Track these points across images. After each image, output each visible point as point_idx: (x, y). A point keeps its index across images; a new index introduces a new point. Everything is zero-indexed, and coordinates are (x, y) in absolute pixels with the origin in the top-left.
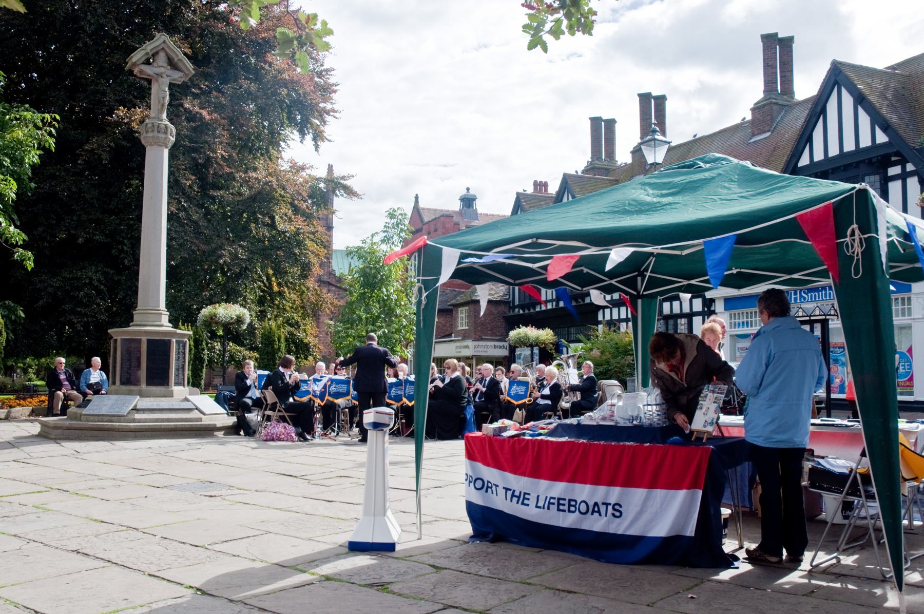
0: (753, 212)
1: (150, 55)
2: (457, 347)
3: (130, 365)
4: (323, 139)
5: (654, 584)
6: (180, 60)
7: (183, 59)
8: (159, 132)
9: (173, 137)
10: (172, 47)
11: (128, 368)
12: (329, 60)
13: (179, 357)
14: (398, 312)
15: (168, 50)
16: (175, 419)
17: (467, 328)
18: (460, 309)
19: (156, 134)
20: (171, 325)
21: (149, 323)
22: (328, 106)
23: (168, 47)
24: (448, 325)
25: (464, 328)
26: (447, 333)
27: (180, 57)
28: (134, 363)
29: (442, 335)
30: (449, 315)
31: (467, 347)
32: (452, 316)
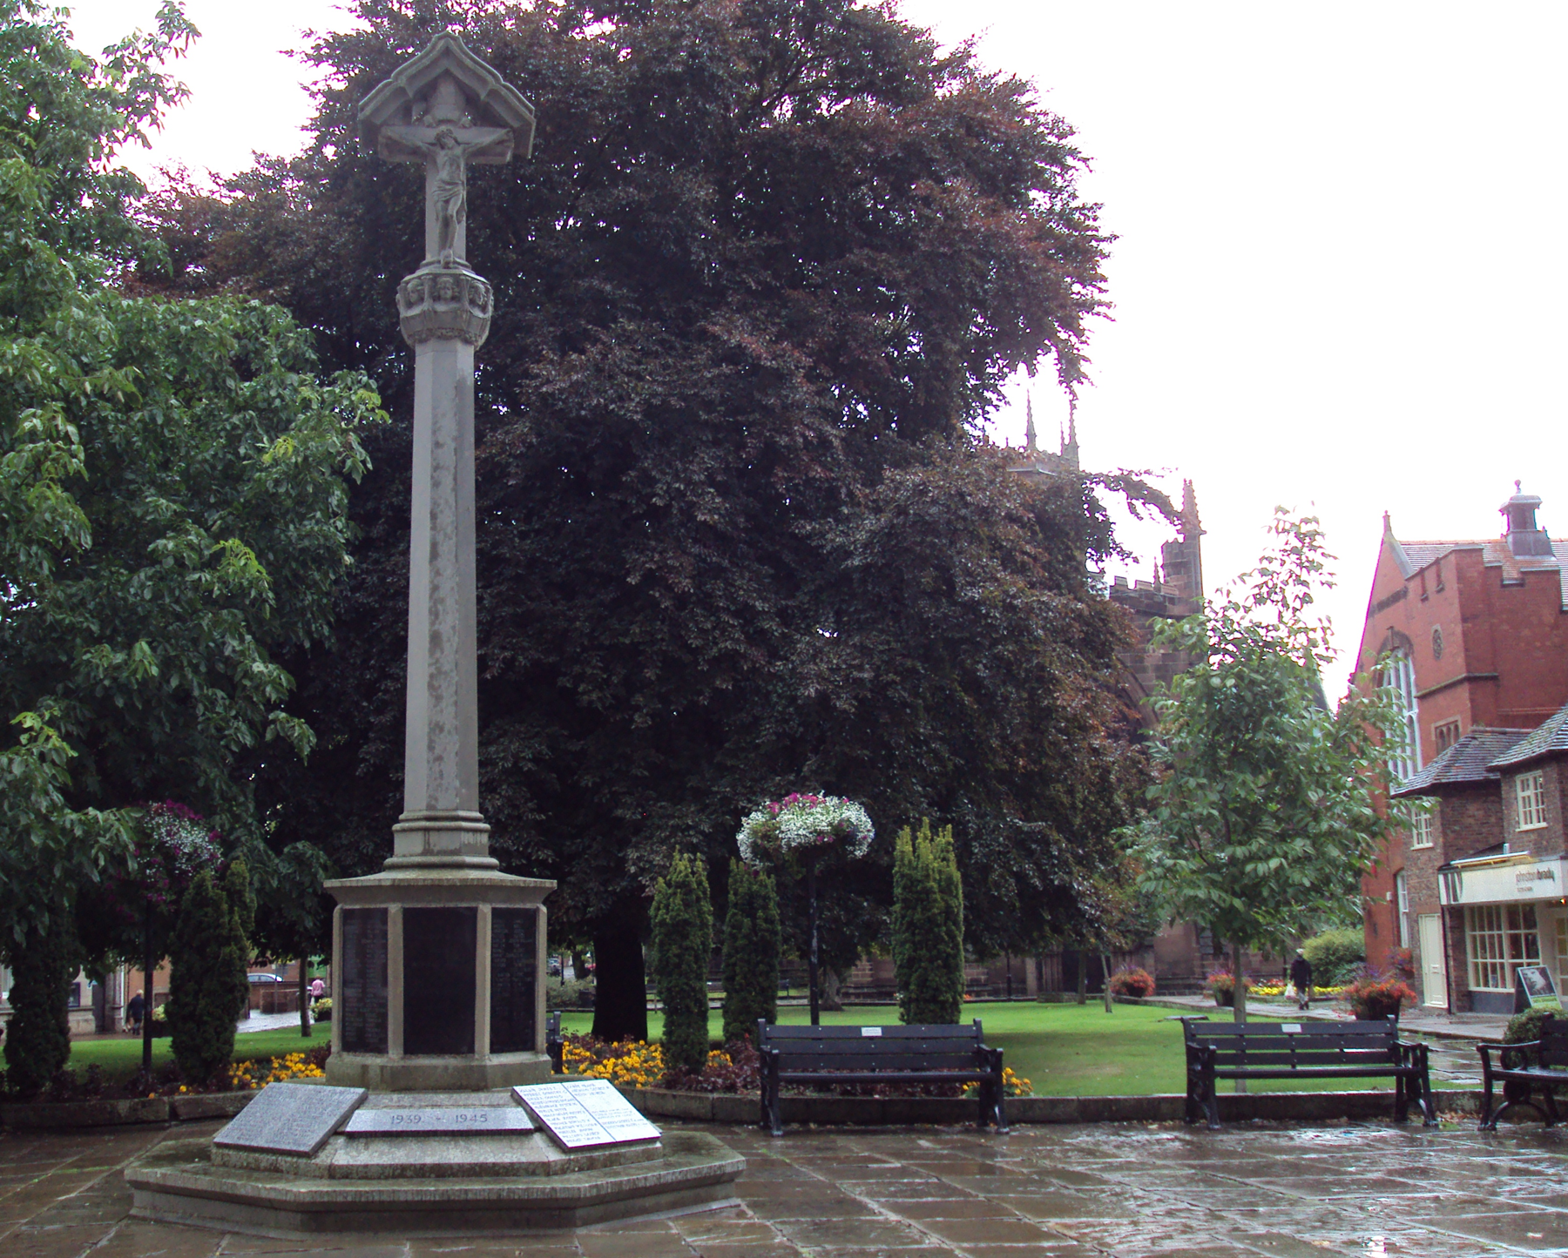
1: (411, 94)
2: (1520, 878)
4: (1081, 377)
6: (493, 93)
7: (504, 92)
9: (484, 309)
10: (468, 62)
12: (1085, 187)
14: (1314, 796)
16: (460, 1166)
17: (1544, 824)
18: (1519, 778)
20: (494, 861)
21: (469, 859)
22: (1090, 293)
23: (461, 64)
24: (1493, 820)
25: (1536, 825)
26: (1492, 841)
29: (1480, 847)
30: (1492, 795)
31: (1549, 875)
32: (1501, 798)
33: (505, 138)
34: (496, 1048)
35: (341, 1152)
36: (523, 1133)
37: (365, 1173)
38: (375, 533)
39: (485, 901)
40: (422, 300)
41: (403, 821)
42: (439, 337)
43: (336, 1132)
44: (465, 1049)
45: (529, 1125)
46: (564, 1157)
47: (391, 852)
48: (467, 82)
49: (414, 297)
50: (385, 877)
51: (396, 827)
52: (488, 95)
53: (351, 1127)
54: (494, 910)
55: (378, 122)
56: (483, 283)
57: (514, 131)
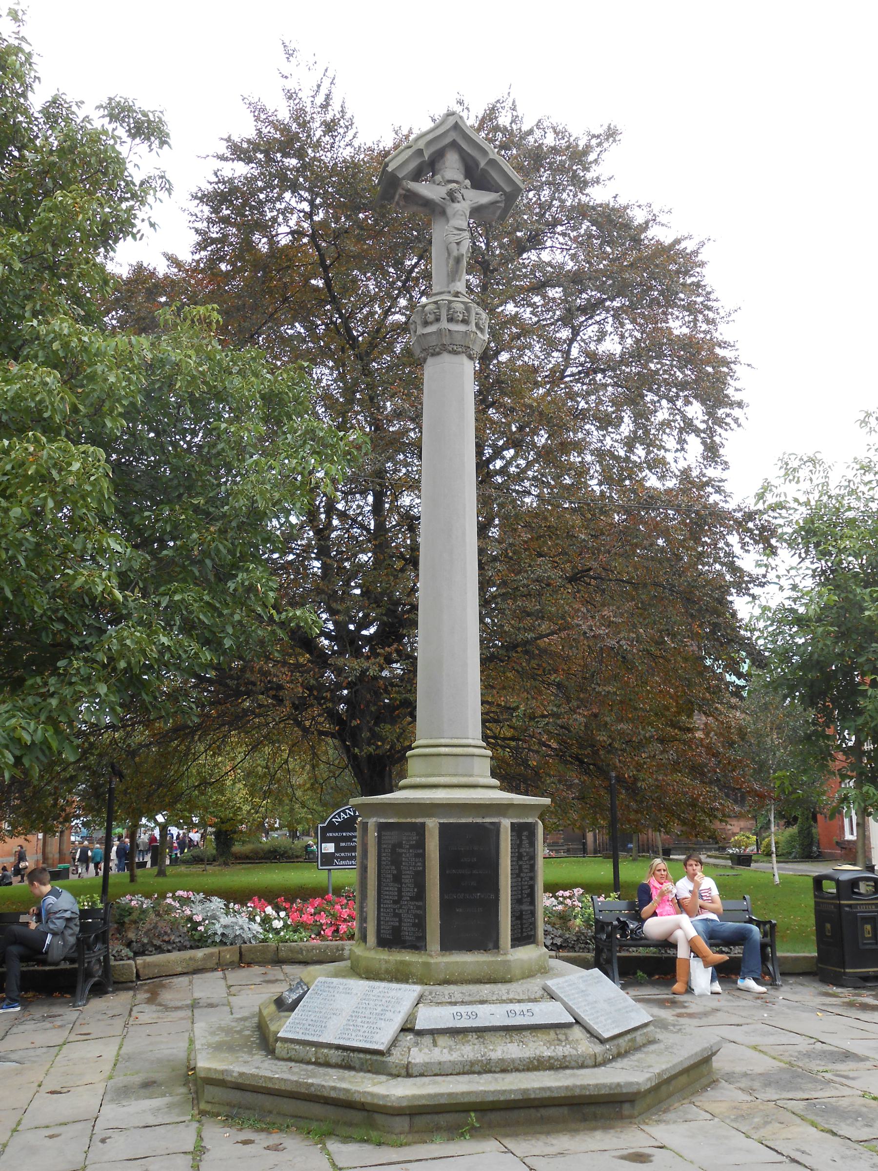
0: (535, 1133)
3: (400, 891)
5: (288, 1127)
8: (451, 320)
11: (395, 902)
13: (520, 867)
15: (464, 146)
19: (444, 324)
20: (496, 782)
27: (491, 156)
28: (409, 890)
35: (414, 1051)
38: (531, 458)
40: (438, 320)
41: (417, 747)
42: (450, 352)
43: (406, 1029)
44: (491, 945)
49: (431, 318)
51: (409, 753)
52: (487, 164)
54: (442, 825)
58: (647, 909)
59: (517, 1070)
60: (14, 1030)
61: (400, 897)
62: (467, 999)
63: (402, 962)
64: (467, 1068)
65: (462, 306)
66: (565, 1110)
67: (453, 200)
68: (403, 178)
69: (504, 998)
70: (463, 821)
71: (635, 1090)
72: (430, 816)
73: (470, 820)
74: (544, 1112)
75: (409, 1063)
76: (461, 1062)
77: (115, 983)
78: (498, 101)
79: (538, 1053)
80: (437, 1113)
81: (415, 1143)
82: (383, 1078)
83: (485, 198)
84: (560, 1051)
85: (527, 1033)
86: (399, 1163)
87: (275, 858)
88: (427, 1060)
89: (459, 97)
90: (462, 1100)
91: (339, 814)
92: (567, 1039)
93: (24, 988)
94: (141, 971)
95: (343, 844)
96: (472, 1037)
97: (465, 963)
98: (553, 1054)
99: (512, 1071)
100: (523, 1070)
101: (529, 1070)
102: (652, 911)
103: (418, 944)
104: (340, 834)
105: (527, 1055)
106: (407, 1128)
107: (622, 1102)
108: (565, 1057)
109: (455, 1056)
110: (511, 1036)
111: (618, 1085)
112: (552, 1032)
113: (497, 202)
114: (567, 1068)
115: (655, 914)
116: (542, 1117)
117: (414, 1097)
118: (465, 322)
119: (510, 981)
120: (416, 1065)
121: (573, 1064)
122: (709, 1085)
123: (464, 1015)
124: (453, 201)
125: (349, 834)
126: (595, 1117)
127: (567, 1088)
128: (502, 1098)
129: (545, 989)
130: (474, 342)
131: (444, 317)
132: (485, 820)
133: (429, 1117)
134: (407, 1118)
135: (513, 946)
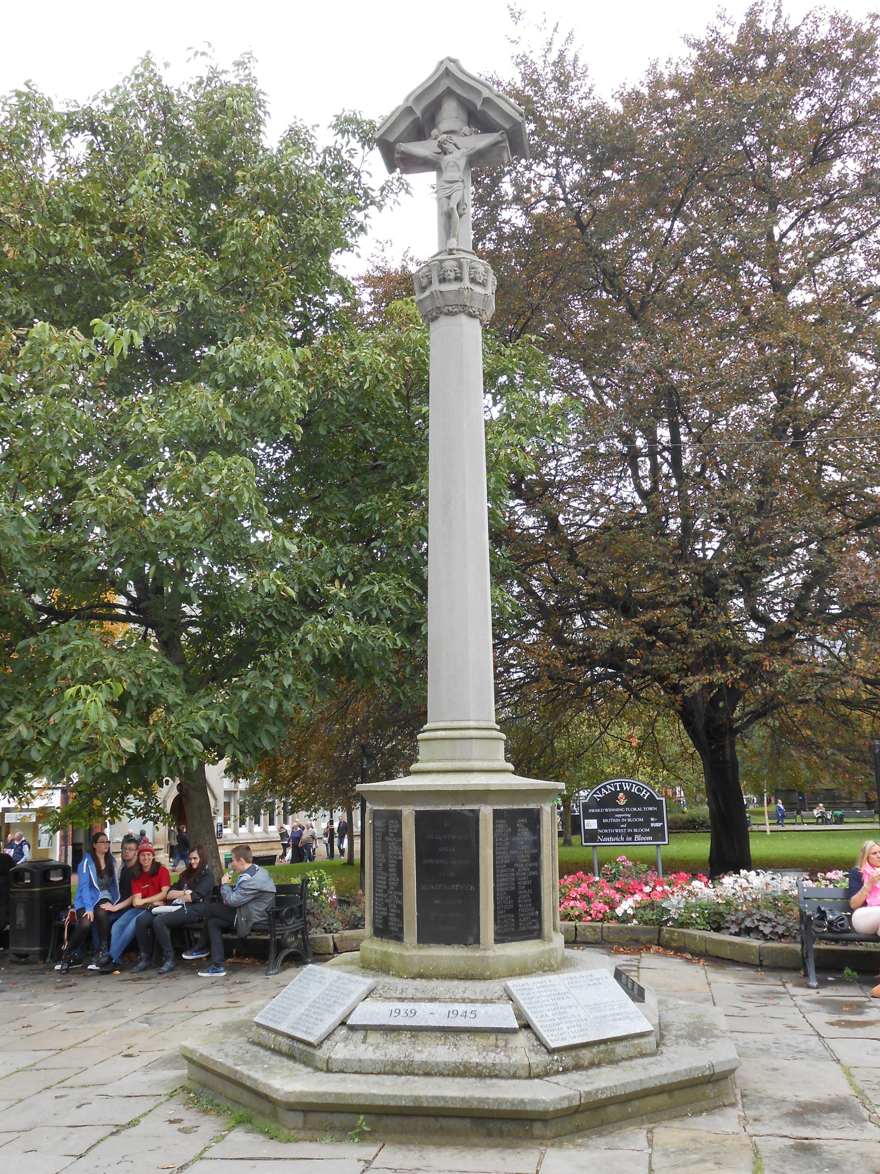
15: (458, 90)
27: (485, 95)
33: (500, 139)
34: (502, 937)
36: (513, 1031)
37: (360, 1069)
39: (486, 803)
42: (446, 314)
43: (343, 1023)
44: (471, 940)
45: (515, 1025)
46: (548, 1058)
47: (413, 759)
48: (464, 95)
50: (402, 783)
51: (419, 736)
53: (349, 1022)
54: (495, 812)
55: (391, 139)
56: (483, 265)
57: (507, 132)
58: (856, 898)
59: (442, 1075)
60: (203, 991)
61: (388, 885)
62: (419, 995)
63: (385, 954)
64: (388, 1068)
65: (454, 263)
66: (468, 1123)
67: (445, 152)
68: (398, 141)
69: (458, 997)
70: (441, 808)
71: (541, 1109)
72: (406, 803)
73: (448, 808)
74: (444, 1122)
75: (330, 1058)
76: (382, 1061)
77: (315, 954)
78: (756, 4)
79: (466, 1058)
80: (332, 1112)
81: (305, 1140)
82: (310, 1070)
83: (483, 141)
84: (492, 1058)
85: (464, 1036)
86: (269, 1159)
87: (694, 828)
88: (348, 1057)
89: (719, 10)
90: (350, 1102)
91: (600, 790)
92: (506, 1046)
93: (228, 954)
94: (338, 945)
95: (605, 821)
96: (405, 1037)
97: (441, 957)
98: (482, 1061)
99: (436, 1075)
100: (448, 1075)
101: (454, 1075)
102: (861, 901)
103: (398, 937)
104: (602, 810)
105: (453, 1060)
106: (300, 1124)
107: (532, 1120)
108: (494, 1065)
109: (378, 1055)
110: (446, 1038)
111: (522, 1101)
112: (492, 1038)
113: (498, 143)
114: (496, 1076)
115: (865, 904)
116: (442, 1128)
117: (301, 1093)
118: (458, 279)
119: (490, 978)
120: (336, 1060)
121: (504, 1073)
122: (718, 1107)
123: (402, 1012)
124: (445, 154)
125: (613, 810)
126: (501, 1134)
127: (463, 1099)
128: (392, 1104)
129: (506, 990)
130: (471, 299)
131: (435, 280)
132: (463, 808)
133: (323, 1115)
134: (300, 1116)
135: (497, 941)
